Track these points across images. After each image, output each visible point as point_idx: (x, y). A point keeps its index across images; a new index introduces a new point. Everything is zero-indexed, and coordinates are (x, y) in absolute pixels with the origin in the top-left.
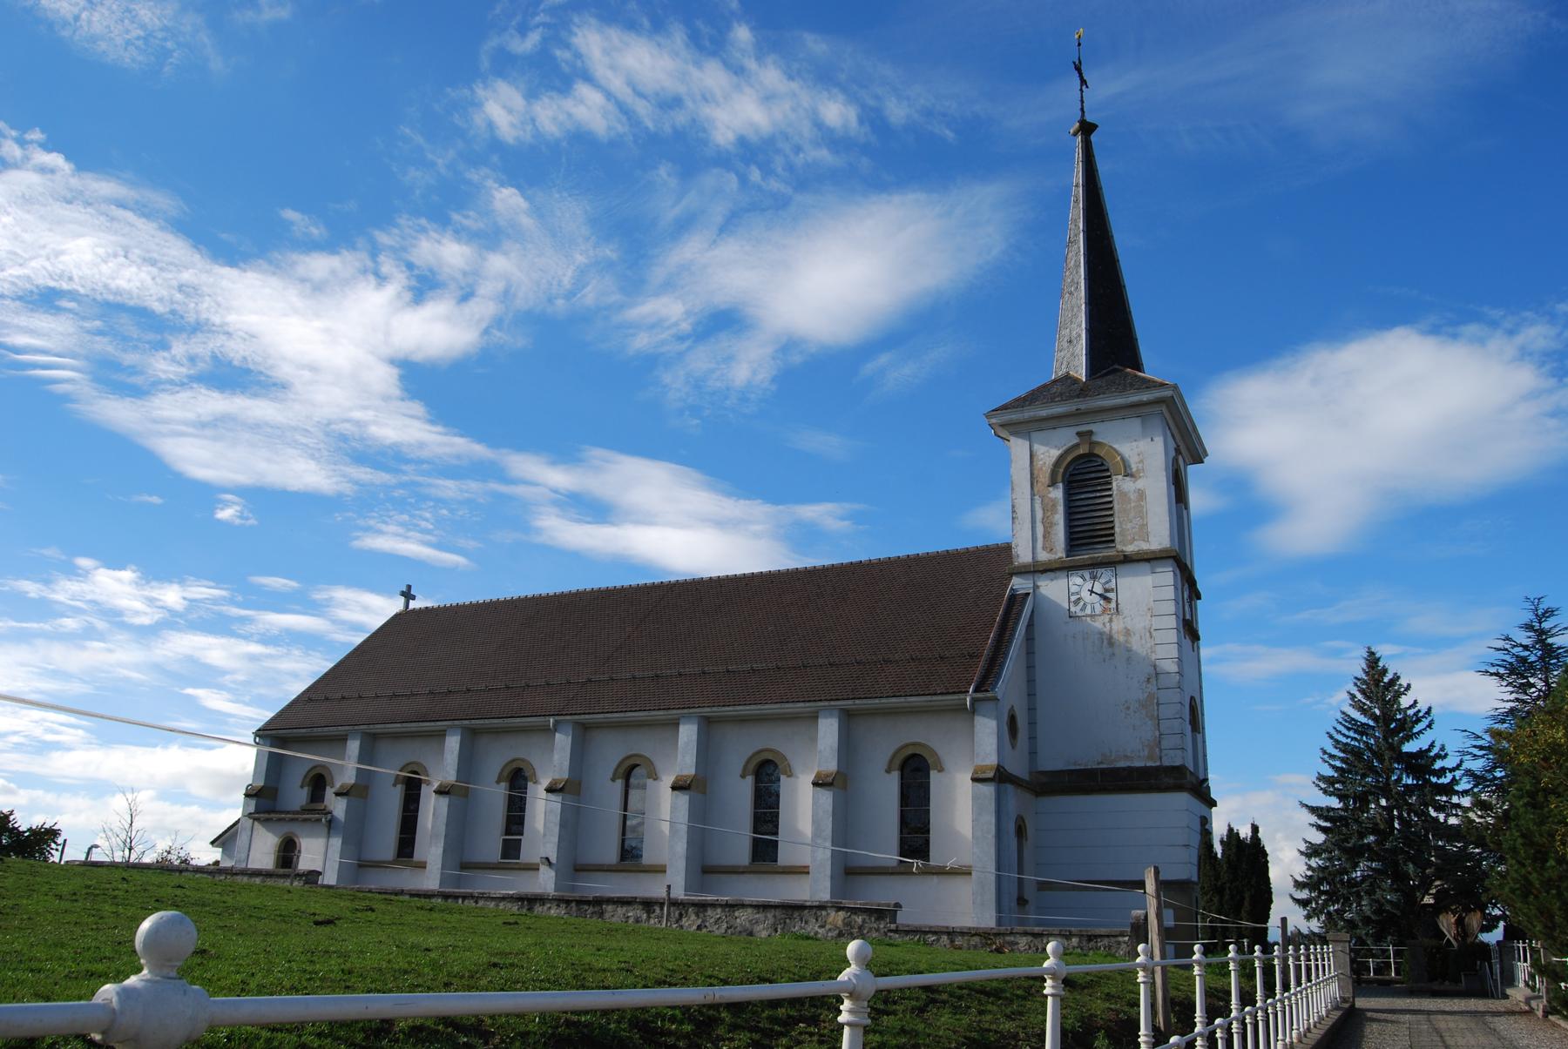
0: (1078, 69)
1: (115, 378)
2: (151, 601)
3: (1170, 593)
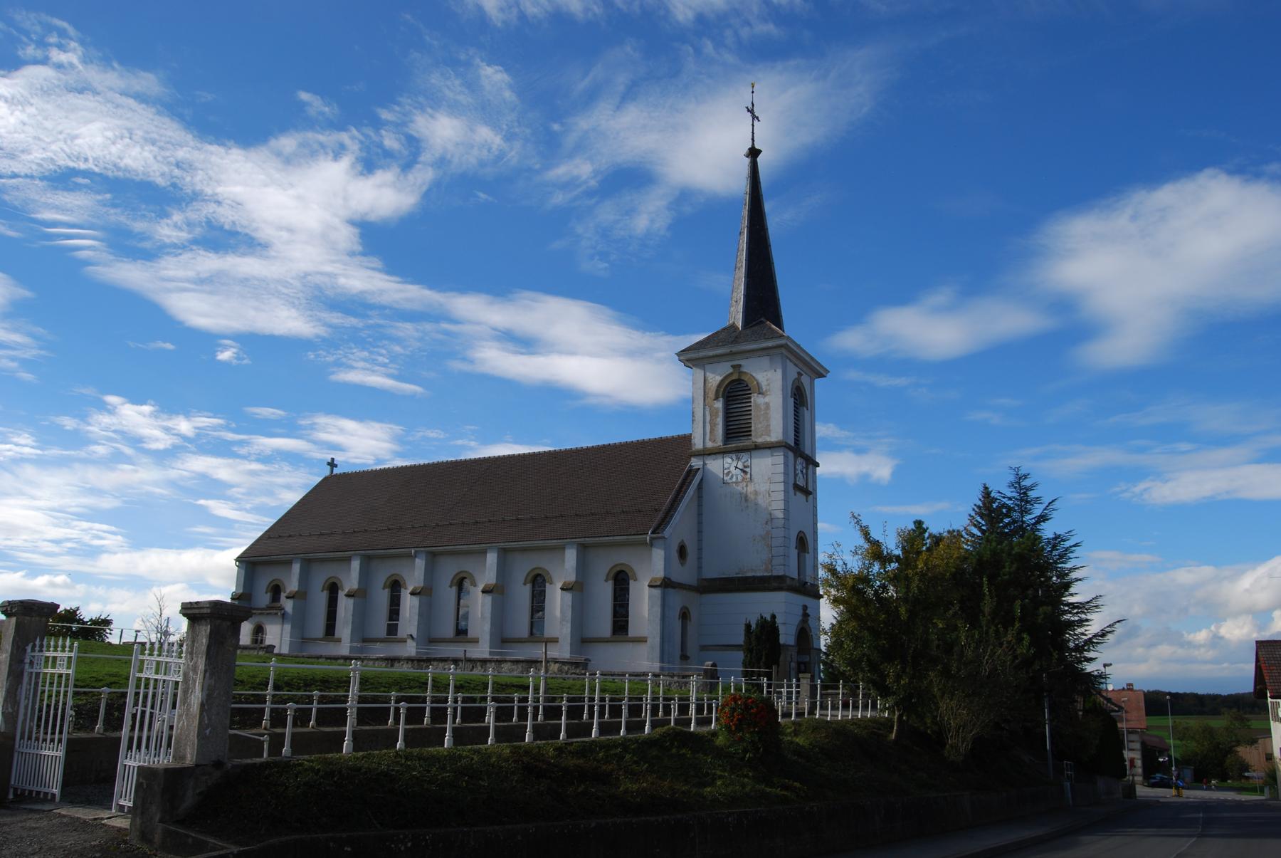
0: (751, 111)
1: (127, 245)
2: (167, 430)
3: (781, 469)
